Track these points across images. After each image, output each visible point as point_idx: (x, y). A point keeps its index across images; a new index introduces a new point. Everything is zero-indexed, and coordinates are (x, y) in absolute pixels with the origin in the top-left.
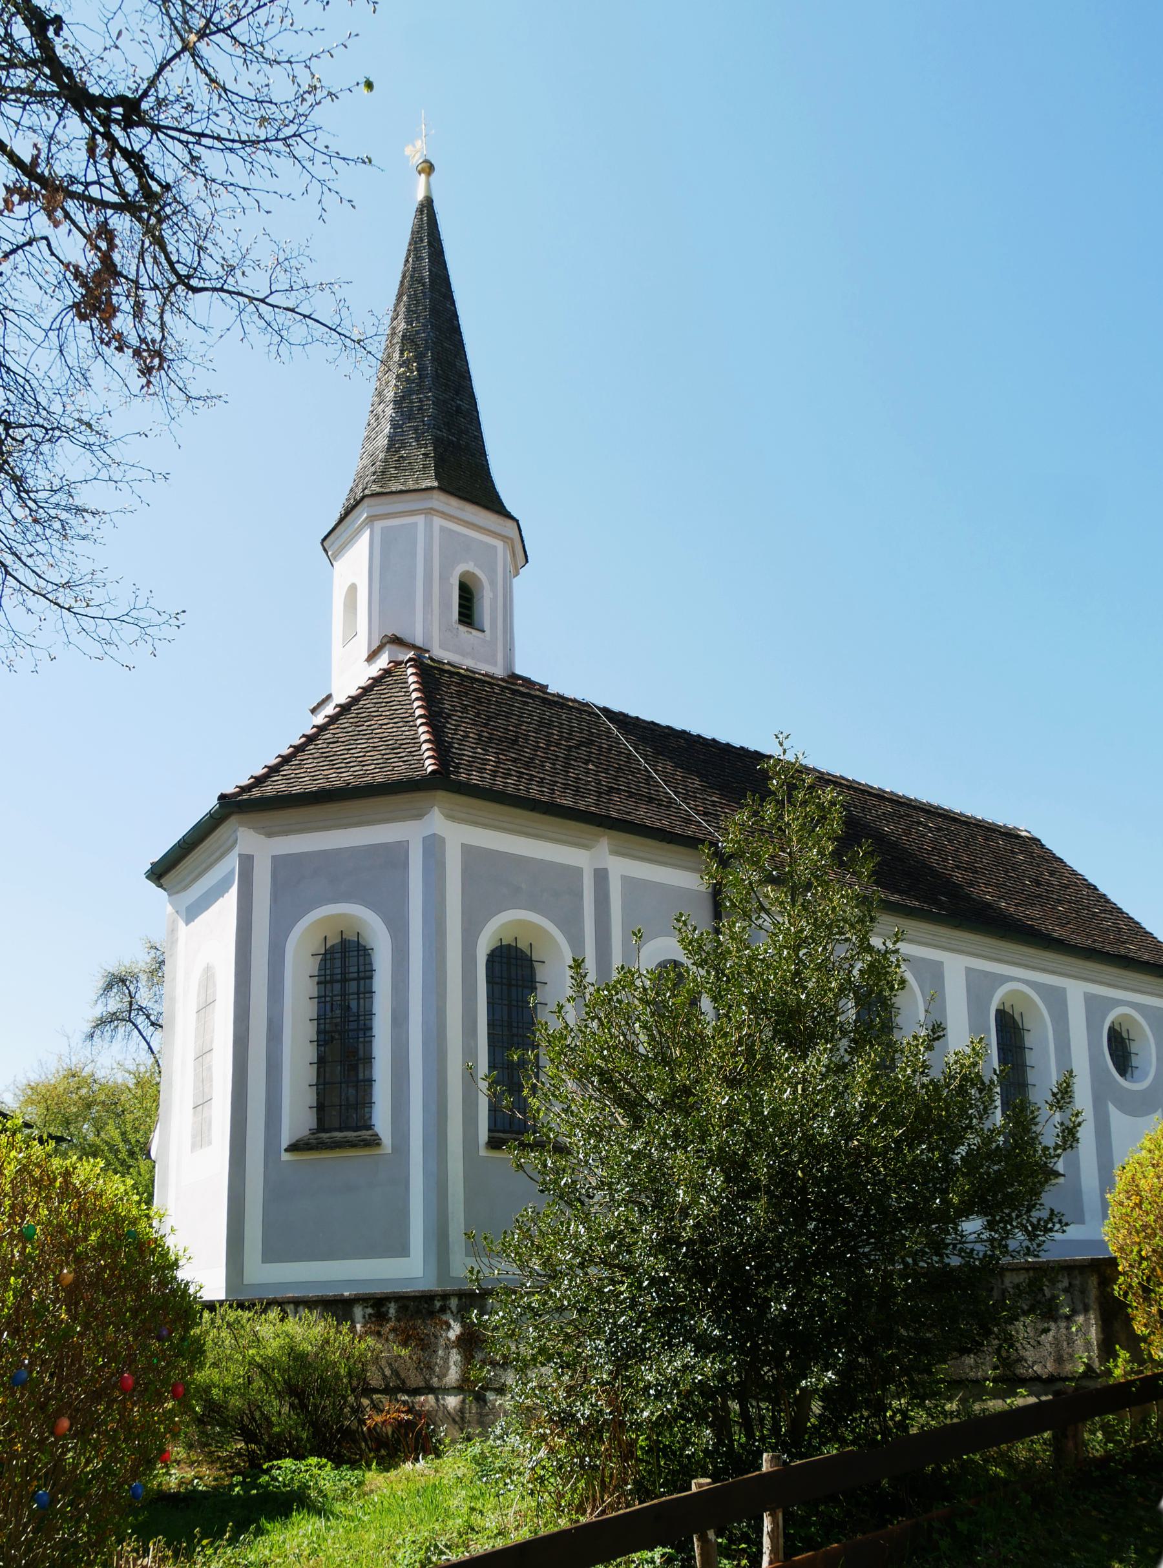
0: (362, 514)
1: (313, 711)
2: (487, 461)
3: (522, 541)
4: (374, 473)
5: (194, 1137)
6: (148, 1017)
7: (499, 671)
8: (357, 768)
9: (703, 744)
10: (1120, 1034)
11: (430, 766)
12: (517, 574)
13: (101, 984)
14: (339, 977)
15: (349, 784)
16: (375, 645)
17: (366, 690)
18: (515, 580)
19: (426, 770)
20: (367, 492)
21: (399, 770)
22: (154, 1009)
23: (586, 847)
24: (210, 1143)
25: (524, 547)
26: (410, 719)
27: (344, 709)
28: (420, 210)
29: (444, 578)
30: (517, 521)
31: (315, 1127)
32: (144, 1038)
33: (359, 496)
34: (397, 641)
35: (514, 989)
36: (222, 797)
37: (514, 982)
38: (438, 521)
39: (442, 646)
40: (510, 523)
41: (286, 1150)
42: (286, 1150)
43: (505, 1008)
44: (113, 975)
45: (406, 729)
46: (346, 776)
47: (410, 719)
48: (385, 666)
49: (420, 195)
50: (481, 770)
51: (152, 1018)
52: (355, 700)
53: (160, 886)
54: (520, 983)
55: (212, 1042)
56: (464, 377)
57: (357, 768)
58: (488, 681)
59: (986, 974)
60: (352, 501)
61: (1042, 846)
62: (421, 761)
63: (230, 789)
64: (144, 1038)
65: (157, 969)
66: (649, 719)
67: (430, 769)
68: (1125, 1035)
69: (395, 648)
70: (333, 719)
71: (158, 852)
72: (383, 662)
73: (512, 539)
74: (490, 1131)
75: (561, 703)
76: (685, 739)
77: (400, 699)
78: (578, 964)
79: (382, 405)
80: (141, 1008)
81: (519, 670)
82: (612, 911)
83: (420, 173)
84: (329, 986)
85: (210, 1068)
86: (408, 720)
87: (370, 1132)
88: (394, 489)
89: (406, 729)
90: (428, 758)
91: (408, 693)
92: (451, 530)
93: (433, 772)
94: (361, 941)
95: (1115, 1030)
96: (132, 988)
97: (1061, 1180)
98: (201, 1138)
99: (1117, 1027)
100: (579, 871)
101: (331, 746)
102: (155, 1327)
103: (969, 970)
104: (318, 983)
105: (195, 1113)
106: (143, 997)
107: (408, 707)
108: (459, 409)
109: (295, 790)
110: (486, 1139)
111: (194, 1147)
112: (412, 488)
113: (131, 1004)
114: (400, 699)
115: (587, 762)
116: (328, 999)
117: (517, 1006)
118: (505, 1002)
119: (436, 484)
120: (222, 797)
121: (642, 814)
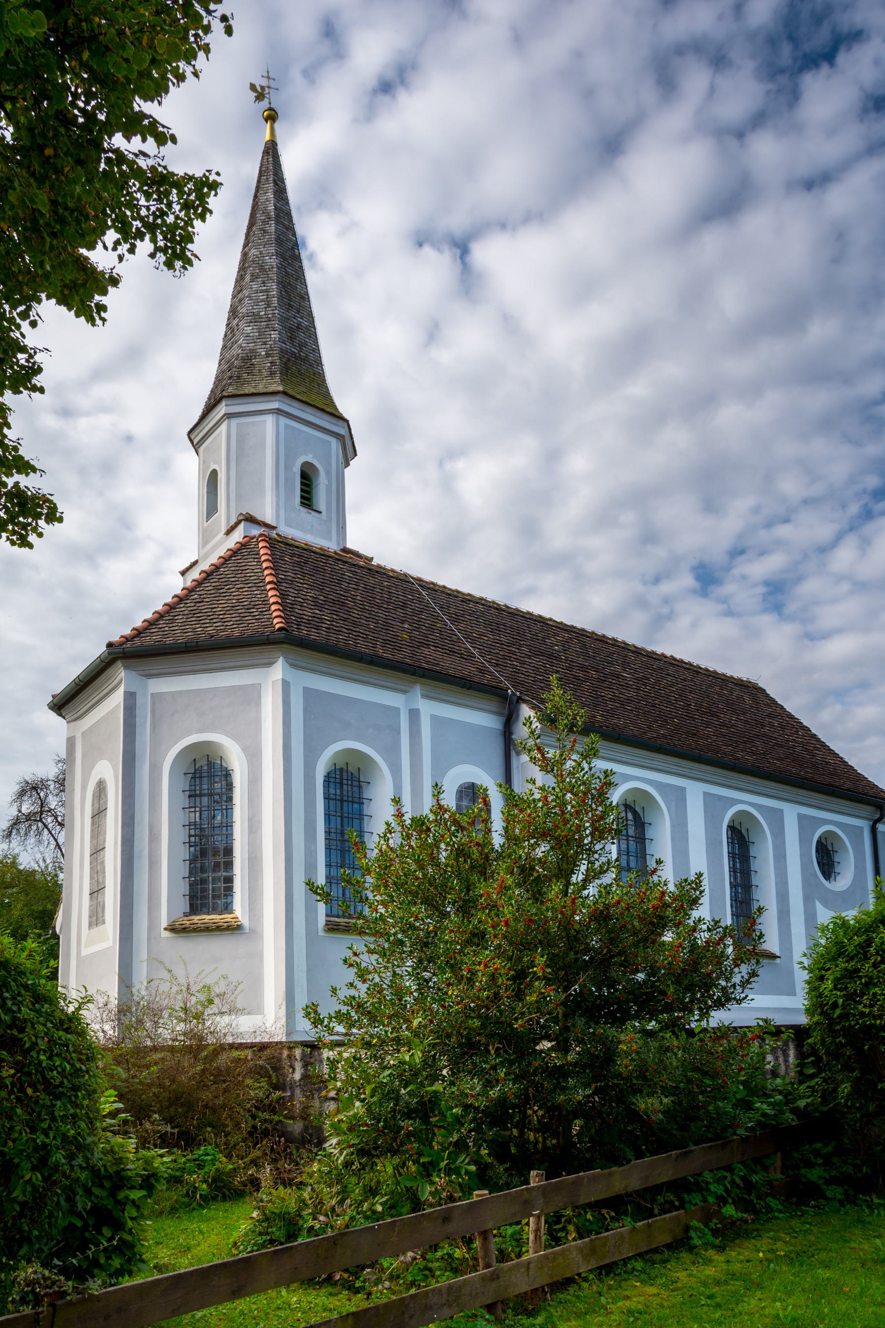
0: (222, 409)
1: (183, 573)
2: (323, 370)
3: (352, 438)
4: (230, 378)
5: (90, 917)
6: (56, 817)
7: (332, 546)
8: (219, 624)
9: (497, 609)
10: (826, 846)
11: (278, 623)
12: (347, 464)
13: (16, 788)
14: (206, 774)
15: (212, 637)
16: (233, 521)
17: (225, 560)
18: (347, 470)
19: (274, 627)
20: (225, 394)
21: (252, 627)
22: (60, 811)
23: (404, 692)
24: (104, 922)
25: (353, 443)
26: (261, 584)
27: (208, 575)
28: (266, 152)
29: (288, 468)
30: (347, 421)
31: (188, 911)
32: (52, 835)
33: (218, 395)
34: (250, 519)
35: (345, 804)
36: (110, 645)
37: (345, 798)
38: (283, 421)
39: (288, 524)
40: (341, 423)
41: (165, 929)
42: (165, 929)
43: (339, 819)
44: (28, 783)
45: (258, 592)
46: (210, 630)
47: (261, 584)
48: (241, 540)
49: (268, 137)
50: (318, 628)
51: (60, 819)
52: (216, 568)
53: (60, 715)
54: (350, 816)
55: (104, 842)
56: (303, 298)
57: (219, 624)
58: (323, 554)
59: (720, 798)
60: (212, 401)
61: (768, 696)
62: (270, 619)
63: (116, 638)
64: (52, 835)
65: (62, 783)
66: (453, 587)
67: (277, 626)
68: (830, 848)
69: (249, 524)
70: (199, 583)
71: (61, 684)
72: (238, 536)
73: (343, 436)
74: (327, 915)
75: (381, 572)
76: (483, 605)
77: (253, 567)
78: (397, 801)
79: (237, 320)
80: (50, 810)
81: (350, 545)
82: (430, 771)
83: (267, 121)
84: (198, 799)
85: (103, 863)
86: (260, 584)
87: (232, 916)
88: (247, 392)
89: (258, 592)
90: (276, 617)
91: (260, 563)
92: (294, 428)
93: (280, 629)
94: (224, 764)
95: (822, 843)
96: (42, 794)
97: (778, 961)
98: (96, 918)
99: (824, 841)
100: (397, 711)
101: (198, 605)
102: (38, 1238)
103: (706, 794)
104: (190, 796)
105: (91, 899)
106: (53, 802)
107: (260, 574)
108: (299, 327)
109: (169, 641)
110: (324, 922)
111: (90, 925)
112: (262, 391)
113: (42, 806)
114: (253, 567)
115: (403, 622)
116: (197, 809)
117: (348, 817)
118: (339, 814)
119: (281, 388)
120: (110, 645)
121: (449, 665)
